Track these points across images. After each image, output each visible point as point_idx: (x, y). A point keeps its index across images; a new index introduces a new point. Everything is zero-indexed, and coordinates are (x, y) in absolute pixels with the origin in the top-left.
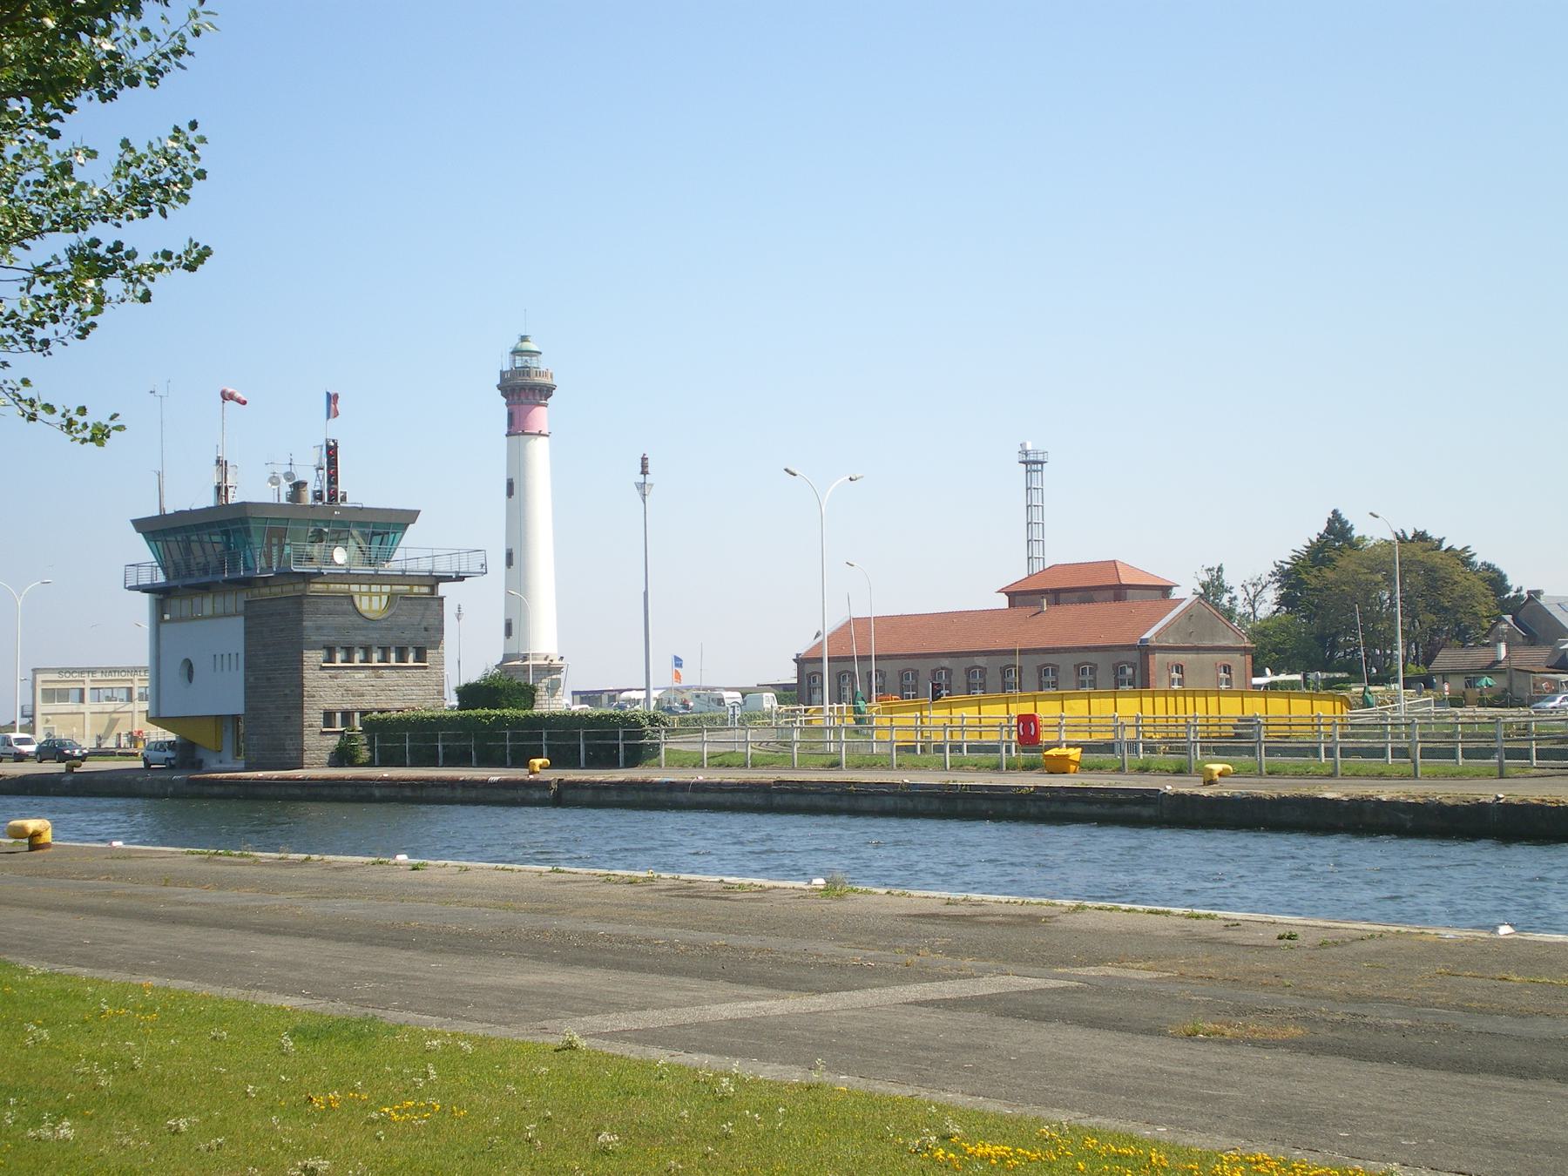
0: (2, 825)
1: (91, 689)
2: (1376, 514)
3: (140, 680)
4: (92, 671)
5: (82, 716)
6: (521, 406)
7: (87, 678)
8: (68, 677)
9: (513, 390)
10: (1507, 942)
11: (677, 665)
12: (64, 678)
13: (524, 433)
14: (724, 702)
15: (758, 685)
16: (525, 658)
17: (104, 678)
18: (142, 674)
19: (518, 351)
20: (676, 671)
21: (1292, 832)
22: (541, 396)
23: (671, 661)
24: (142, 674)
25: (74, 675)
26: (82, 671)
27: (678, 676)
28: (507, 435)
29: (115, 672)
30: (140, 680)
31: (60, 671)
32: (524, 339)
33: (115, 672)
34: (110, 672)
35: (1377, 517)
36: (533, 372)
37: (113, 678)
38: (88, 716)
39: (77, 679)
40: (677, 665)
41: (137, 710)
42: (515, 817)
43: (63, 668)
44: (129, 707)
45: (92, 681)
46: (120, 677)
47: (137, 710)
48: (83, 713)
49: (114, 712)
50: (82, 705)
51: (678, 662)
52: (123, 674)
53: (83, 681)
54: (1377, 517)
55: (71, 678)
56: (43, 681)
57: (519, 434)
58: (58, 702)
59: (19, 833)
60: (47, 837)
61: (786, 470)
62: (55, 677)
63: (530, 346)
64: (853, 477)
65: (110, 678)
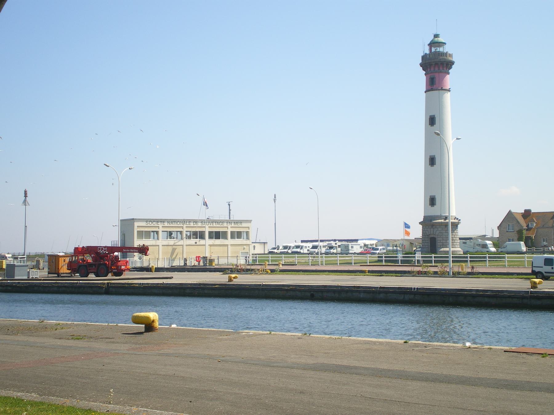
0: (553, 347)
1: (162, 231)
2: (199, 194)
3: (186, 227)
4: (162, 221)
5: (226, 248)
6: (440, 74)
7: (161, 225)
8: (150, 224)
9: (430, 65)
10: (174, 328)
11: (406, 227)
12: (149, 225)
13: (442, 89)
14: (487, 246)
15: (415, 239)
16: (446, 218)
17: (169, 225)
18: (188, 223)
19: (434, 43)
20: (406, 230)
21: (155, 296)
22: (446, 69)
23: (402, 225)
24: (188, 223)
25: (154, 223)
26: (158, 221)
27: (408, 234)
28: (425, 92)
29: (174, 222)
30: (186, 227)
31: (147, 221)
32: (436, 36)
33: (174, 222)
34: (172, 222)
35: (199, 195)
36: (448, 55)
37: (173, 226)
38: (161, 247)
39: (155, 225)
40: (406, 227)
41: (185, 244)
42: (243, 303)
43: (148, 219)
44: (181, 243)
45: (163, 227)
46: (177, 225)
47: (185, 244)
48: (159, 246)
49: (173, 245)
50: (158, 241)
51: (407, 226)
52: (178, 223)
53: (228, 227)
54: (199, 195)
55: (152, 225)
56: (138, 226)
57: (439, 90)
58: (145, 239)
59: (137, 320)
60: (157, 325)
61: (105, 164)
62: (144, 224)
63: (440, 39)
64: (131, 168)
65: (172, 225)
